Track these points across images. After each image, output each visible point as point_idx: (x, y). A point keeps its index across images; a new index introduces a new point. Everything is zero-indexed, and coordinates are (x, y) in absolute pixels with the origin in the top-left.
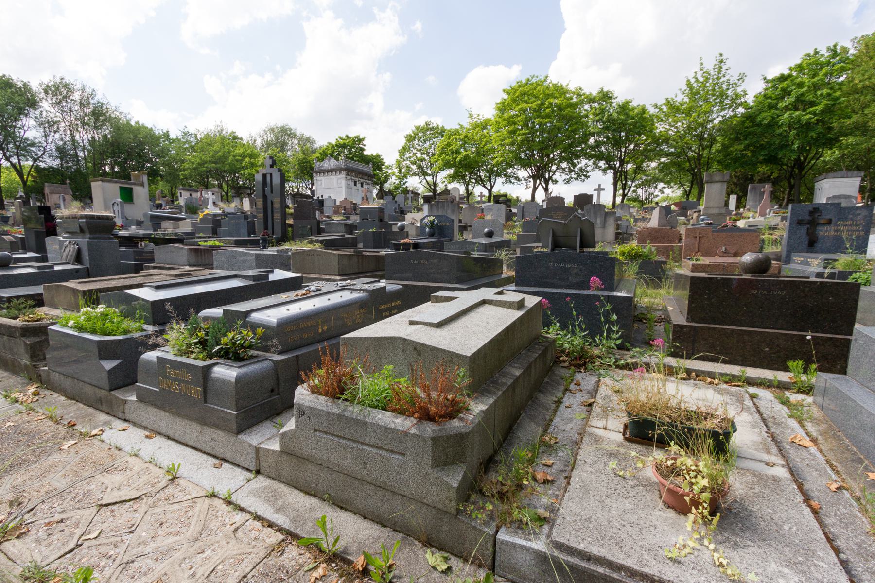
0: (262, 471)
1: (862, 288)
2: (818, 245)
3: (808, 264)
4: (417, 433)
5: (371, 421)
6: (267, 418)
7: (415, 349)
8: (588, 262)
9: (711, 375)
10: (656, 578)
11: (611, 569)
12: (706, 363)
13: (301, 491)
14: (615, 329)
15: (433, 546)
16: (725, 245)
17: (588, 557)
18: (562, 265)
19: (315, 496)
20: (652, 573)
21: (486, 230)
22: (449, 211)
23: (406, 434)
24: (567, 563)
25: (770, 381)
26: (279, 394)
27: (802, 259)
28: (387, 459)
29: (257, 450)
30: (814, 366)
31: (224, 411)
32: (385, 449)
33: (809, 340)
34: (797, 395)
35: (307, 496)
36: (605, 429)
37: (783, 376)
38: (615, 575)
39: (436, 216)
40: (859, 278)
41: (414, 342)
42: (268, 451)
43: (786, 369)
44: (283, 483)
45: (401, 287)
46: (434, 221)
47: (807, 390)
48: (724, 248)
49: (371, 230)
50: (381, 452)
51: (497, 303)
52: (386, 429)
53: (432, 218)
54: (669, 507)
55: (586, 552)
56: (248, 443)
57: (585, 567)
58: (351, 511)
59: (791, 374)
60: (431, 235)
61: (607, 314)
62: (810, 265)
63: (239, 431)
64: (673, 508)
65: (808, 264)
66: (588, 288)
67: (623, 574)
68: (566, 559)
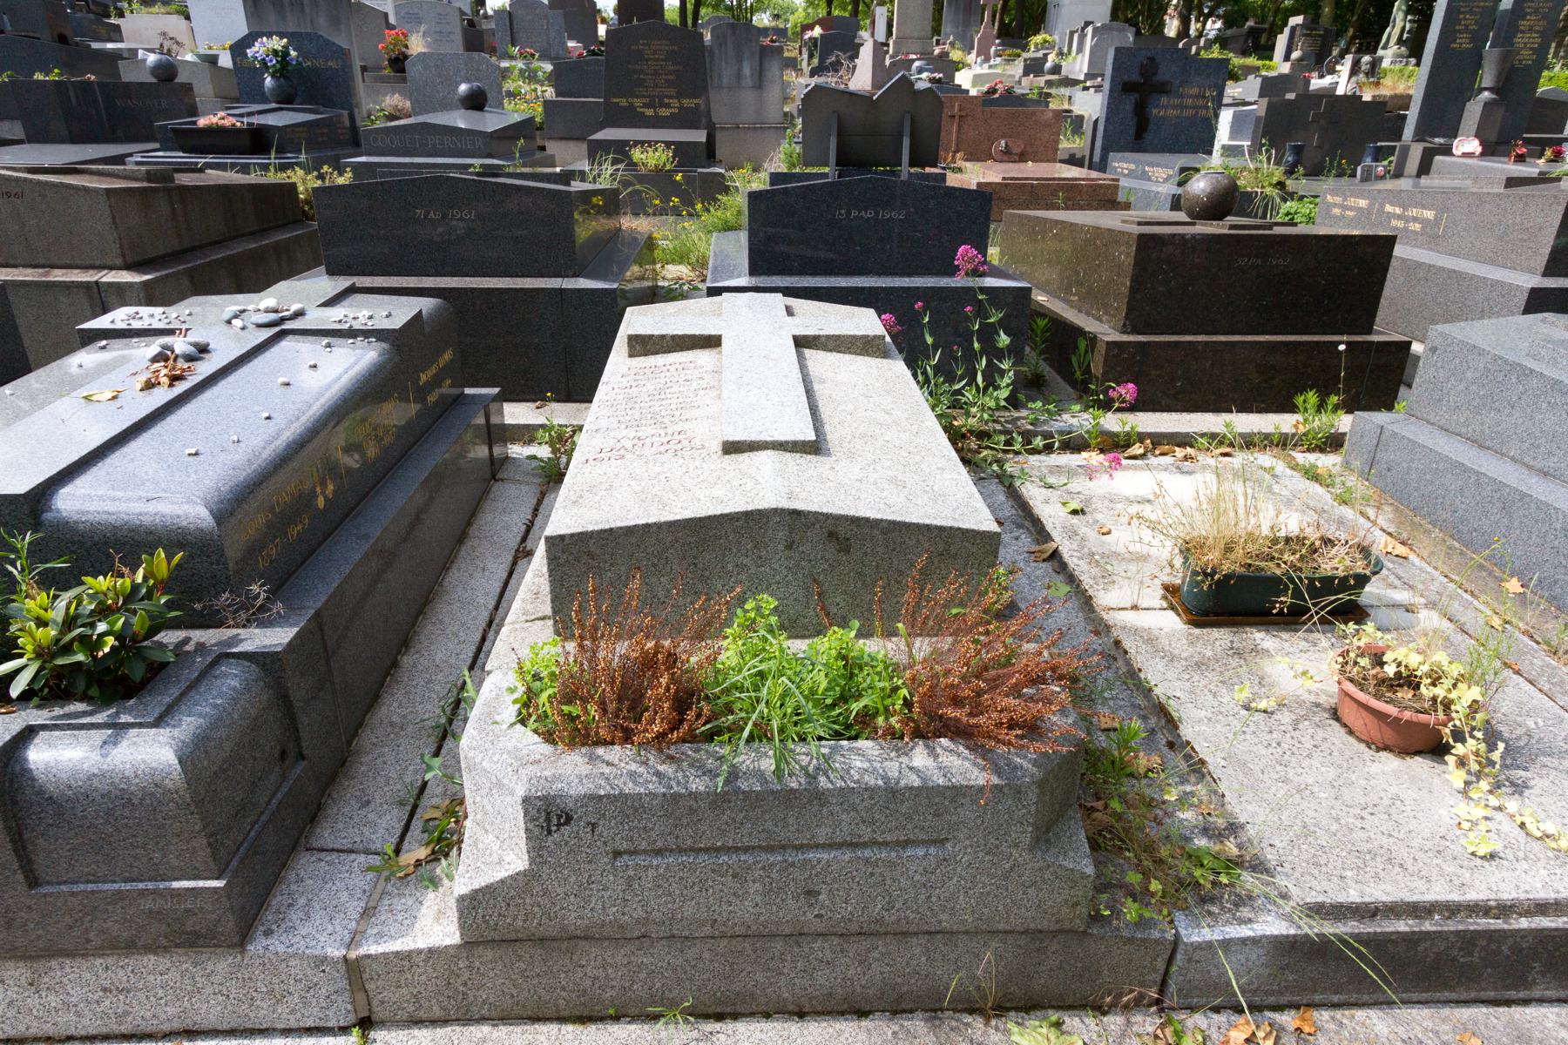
0: (379, 1013)
1: (1398, 250)
2: (1149, 137)
3: (1145, 176)
4: (995, 780)
5: (840, 783)
6: (293, 848)
7: (832, 535)
8: (932, 204)
9: (1183, 440)
10: (1492, 903)
11: (1416, 917)
12: (1158, 415)
13: (562, 1020)
14: (1005, 366)
15: (1008, 1010)
16: (1003, 137)
17: (1369, 911)
18: (868, 214)
19: (616, 1019)
20: (1485, 898)
21: (463, 88)
22: (322, 20)
23: (957, 793)
24: (1358, 937)
25: (1267, 436)
26: (302, 757)
27: (1133, 166)
28: (891, 865)
29: (354, 970)
30: (1334, 399)
31: (154, 892)
32: (885, 844)
33: (1341, 352)
34: (1307, 455)
35: (592, 1028)
36: (1135, 607)
37: (1284, 423)
38: (1428, 926)
39: (294, 38)
40: (1296, 213)
41: (827, 516)
42: (406, 958)
43: (1293, 409)
44: (483, 1020)
45: (426, 304)
46: (286, 54)
47: (1334, 442)
48: (1003, 143)
49: (38, 76)
50: (867, 853)
51: (831, 344)
52: (893, 793)
53: (277, 43)
54: (1378, 749)
55: (1367, 904)
56: (302, 957)
57: (1375, 933)
58: (752, 1015)
59: (1298, 417)
60: (286, 99)
61: (988, 334)
62: (1149, 179)
63: (241, 940)
64: (1386, 748)
65: (1145, 176)
66: (952, 271)
67: (1437, 917)
68: (1337, 931)
